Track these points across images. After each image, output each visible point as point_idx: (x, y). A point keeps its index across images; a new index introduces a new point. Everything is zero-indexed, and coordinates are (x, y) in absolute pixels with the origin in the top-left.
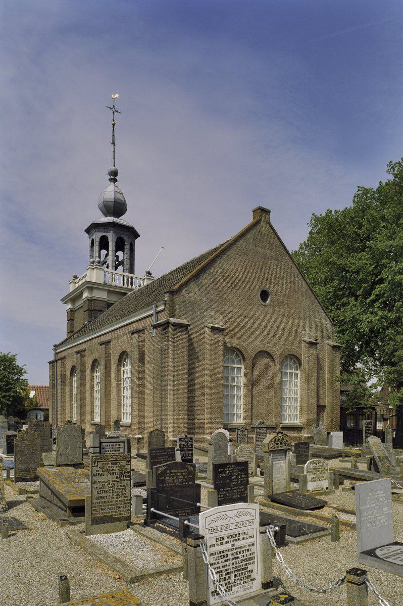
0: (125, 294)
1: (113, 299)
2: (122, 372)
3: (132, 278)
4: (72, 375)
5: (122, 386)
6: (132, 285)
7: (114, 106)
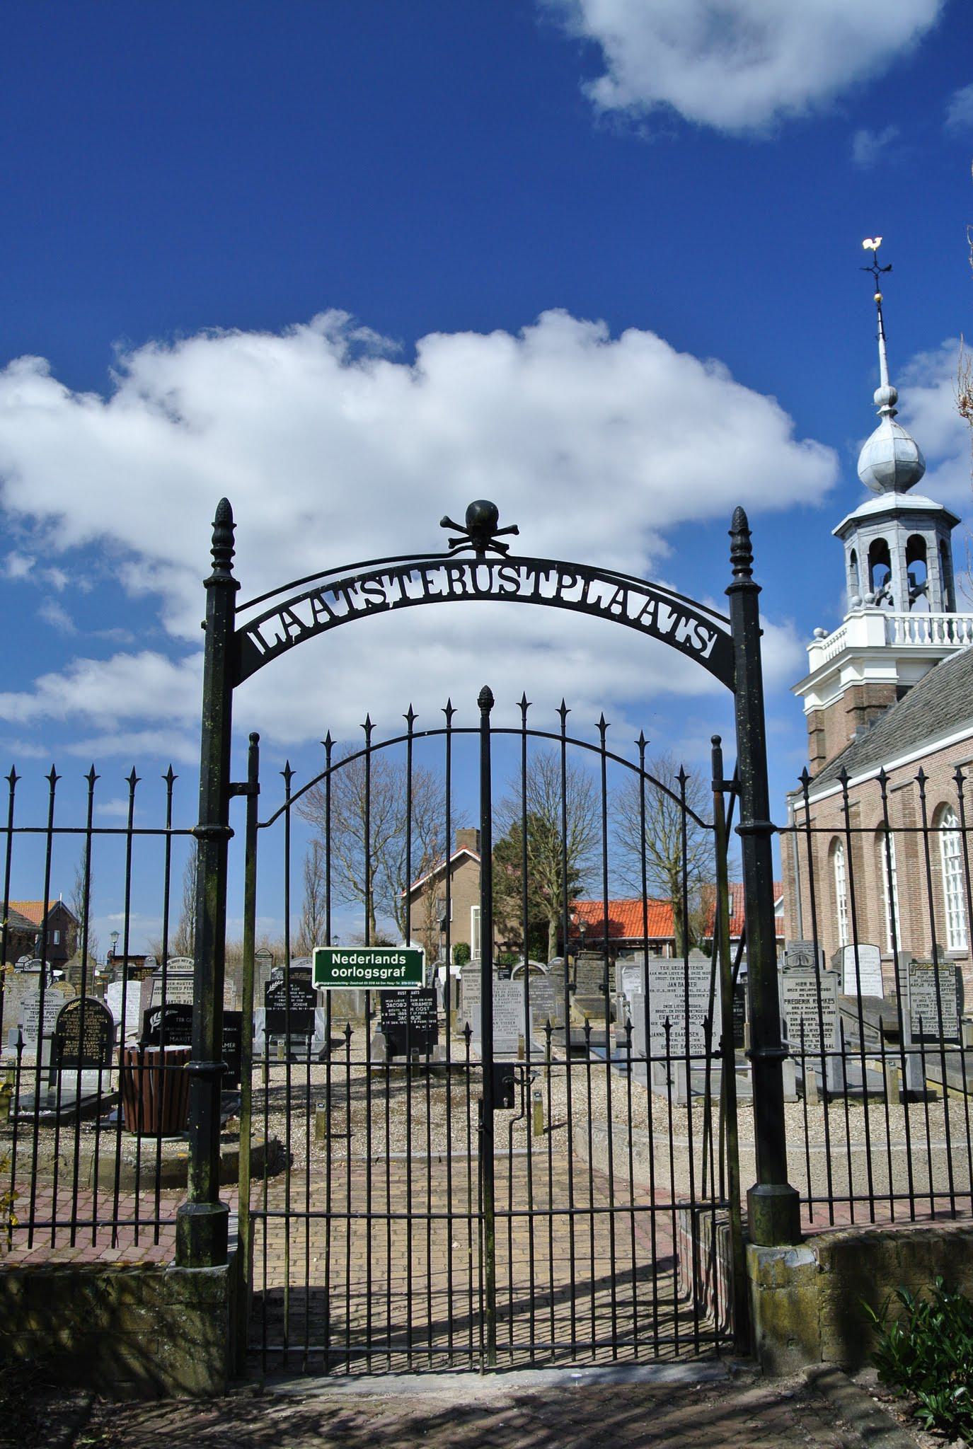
0: (935, 662)
1: (913, 676)
2: (942, 845)
3: (950, 623)
4: (832, 851)
5: (944, 874)
6: (951, 635)
7: (876, 263)
